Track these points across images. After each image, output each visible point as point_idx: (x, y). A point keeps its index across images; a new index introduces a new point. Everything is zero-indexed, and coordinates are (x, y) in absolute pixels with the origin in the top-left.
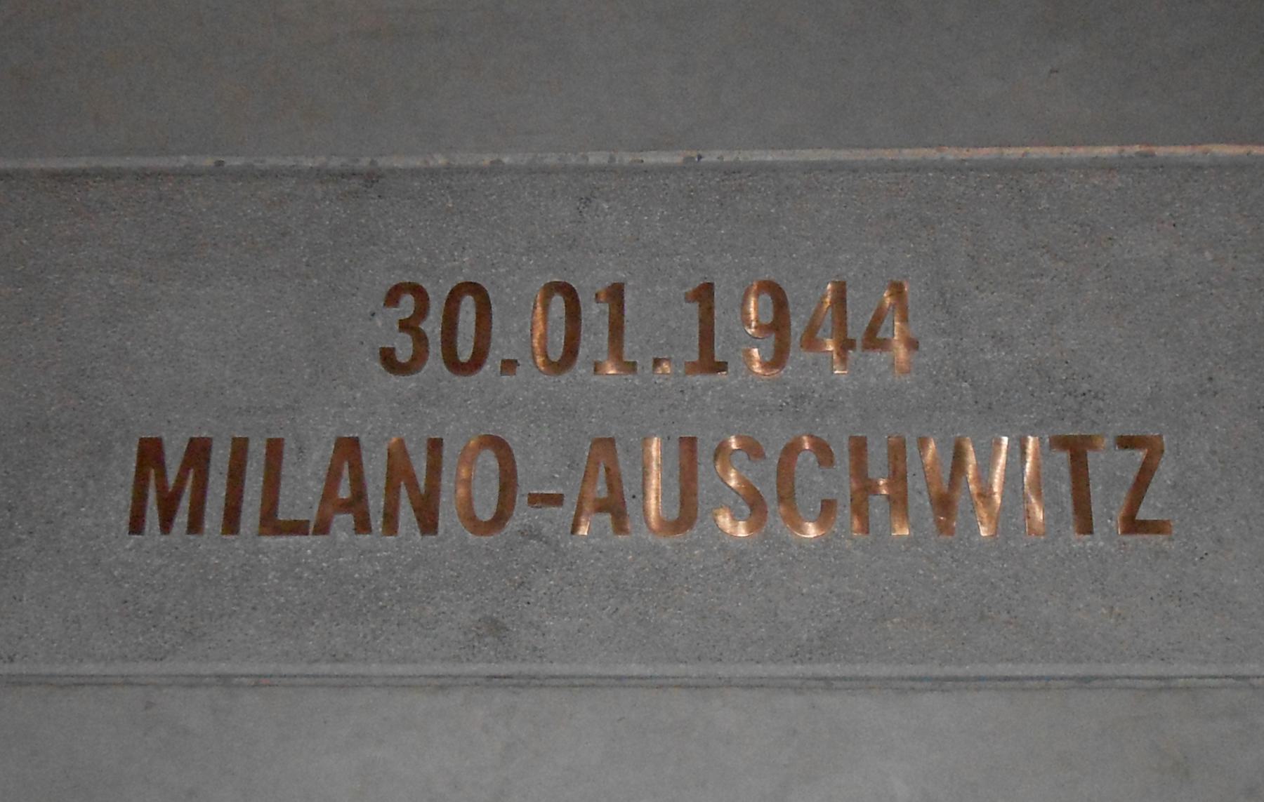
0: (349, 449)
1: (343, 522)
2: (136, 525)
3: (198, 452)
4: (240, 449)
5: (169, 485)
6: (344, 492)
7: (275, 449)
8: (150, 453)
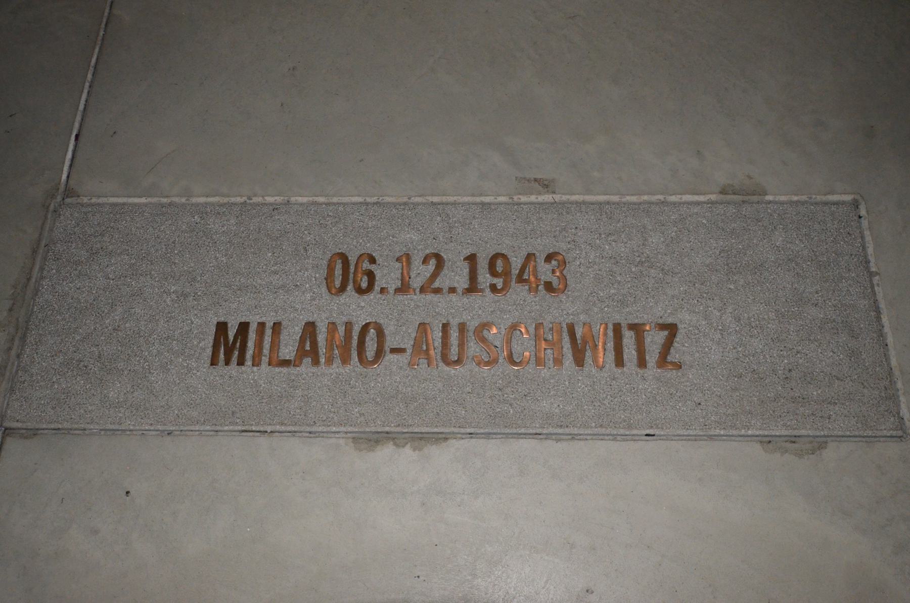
0: (310, 328)
1: (308, 360)
2: (214, 362)
3: (244, 328)
4: (262, 325)
5: (230, 344)
6: (308, 348)
7: (277, 326)
8: (222, 327)
